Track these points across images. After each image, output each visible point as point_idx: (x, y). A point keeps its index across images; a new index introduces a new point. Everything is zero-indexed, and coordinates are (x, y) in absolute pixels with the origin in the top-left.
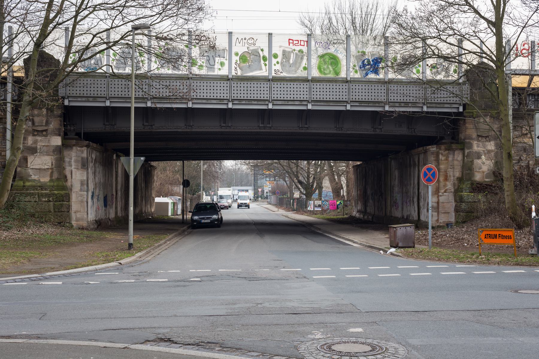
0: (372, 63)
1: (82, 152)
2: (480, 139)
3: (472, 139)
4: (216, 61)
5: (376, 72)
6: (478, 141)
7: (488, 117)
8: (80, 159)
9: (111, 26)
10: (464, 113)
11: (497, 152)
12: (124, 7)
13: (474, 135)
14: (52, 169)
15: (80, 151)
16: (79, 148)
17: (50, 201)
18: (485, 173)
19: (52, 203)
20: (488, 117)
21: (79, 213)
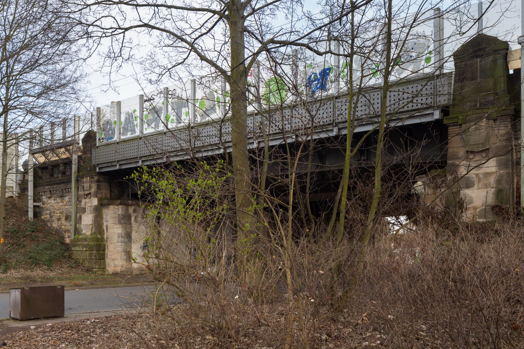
0: (319, 77)
1: (118, 209)
2: (471, 156)
3: (458, 158)
4: (183, 112)
5: (323, 87)
6: (467, 159)
7: (485, 119)
8: (117, 215)
9: (355, 14)
10: (444, 120)
11: (501, 176)
12: (22, 122)
13: (462, 152)
14: (92, 224)
15: (117, 209)
16: (116, 207)
17: (87, 251)
18: (478, 210)
19: (88, 252)
20: (485, 119)
21: (117, 261)
